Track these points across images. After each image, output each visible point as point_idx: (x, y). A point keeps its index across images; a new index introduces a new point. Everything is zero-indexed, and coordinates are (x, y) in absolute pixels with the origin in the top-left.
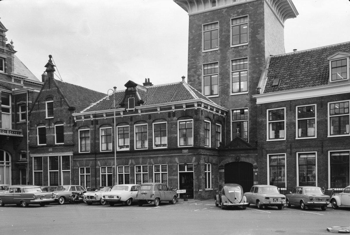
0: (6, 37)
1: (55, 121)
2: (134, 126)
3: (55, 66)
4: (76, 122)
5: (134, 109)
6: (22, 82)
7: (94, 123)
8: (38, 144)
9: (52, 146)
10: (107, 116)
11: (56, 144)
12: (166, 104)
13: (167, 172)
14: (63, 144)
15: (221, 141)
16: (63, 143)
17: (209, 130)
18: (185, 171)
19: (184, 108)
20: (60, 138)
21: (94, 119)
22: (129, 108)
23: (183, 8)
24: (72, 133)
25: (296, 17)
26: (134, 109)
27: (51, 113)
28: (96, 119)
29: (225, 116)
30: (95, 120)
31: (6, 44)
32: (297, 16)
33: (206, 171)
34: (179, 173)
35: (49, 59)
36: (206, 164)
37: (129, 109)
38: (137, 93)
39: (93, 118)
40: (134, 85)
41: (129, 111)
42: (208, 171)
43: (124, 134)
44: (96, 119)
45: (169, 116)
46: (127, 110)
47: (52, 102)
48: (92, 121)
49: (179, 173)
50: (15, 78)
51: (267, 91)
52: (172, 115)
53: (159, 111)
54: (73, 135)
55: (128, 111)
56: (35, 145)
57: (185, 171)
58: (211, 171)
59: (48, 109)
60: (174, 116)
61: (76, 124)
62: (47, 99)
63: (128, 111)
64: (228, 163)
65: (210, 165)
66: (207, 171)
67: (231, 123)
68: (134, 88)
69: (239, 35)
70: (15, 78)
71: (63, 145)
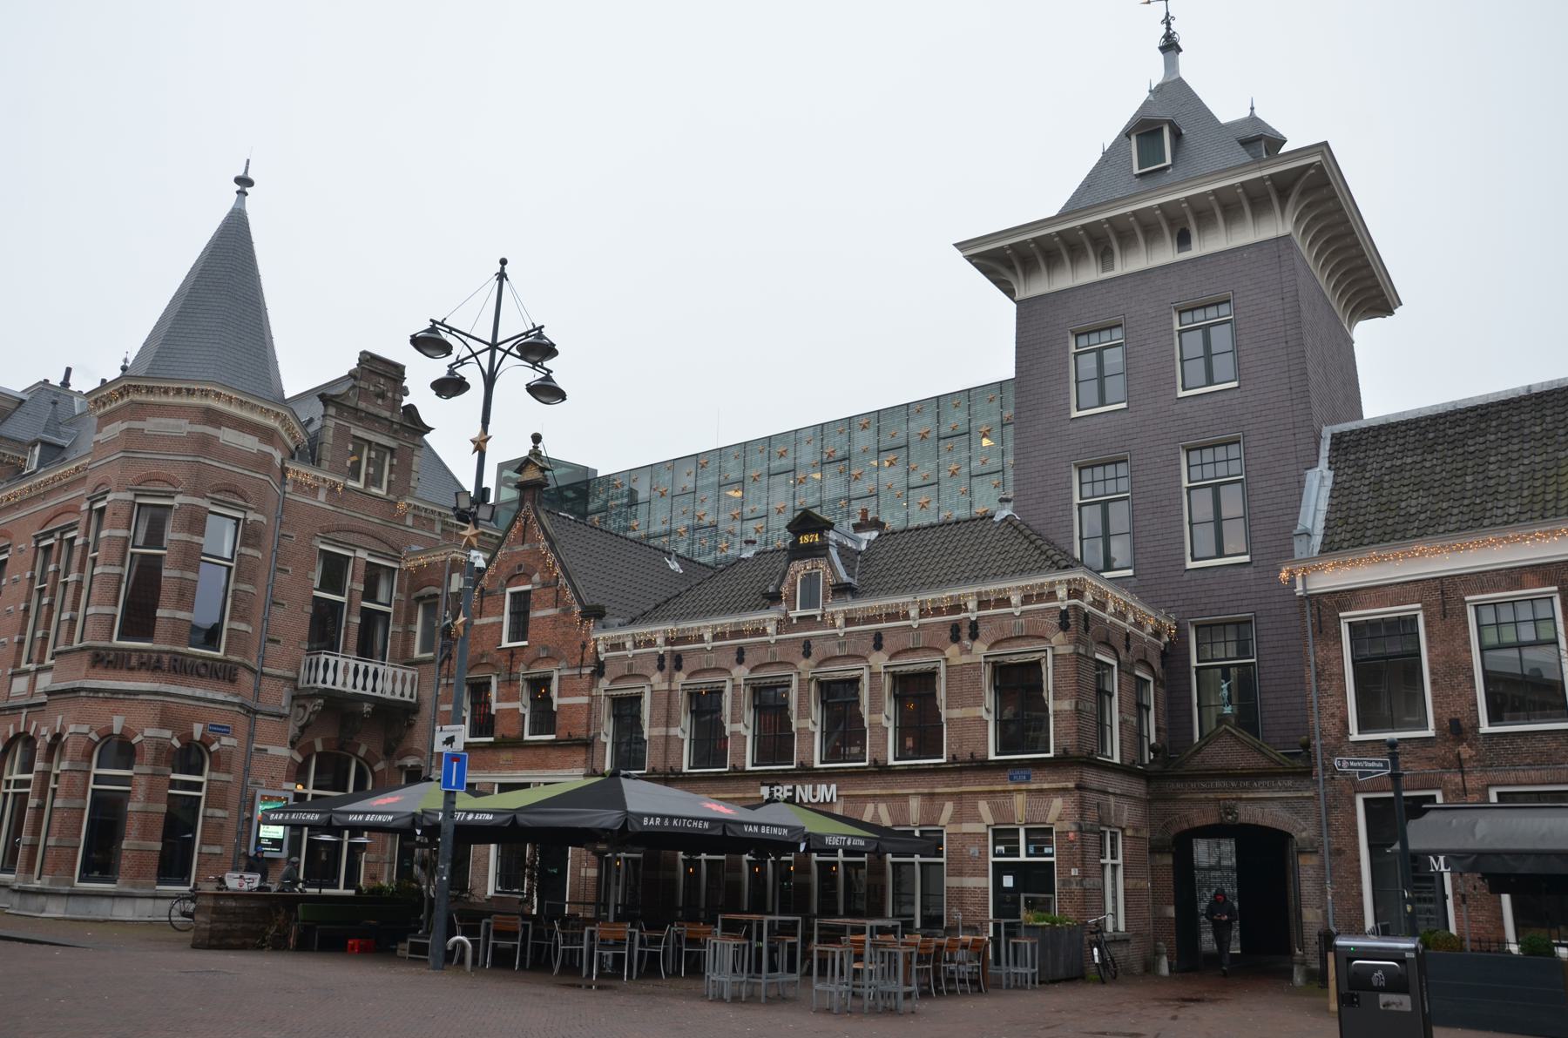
0: (404, 384)
1: (529, 654)
2: (584, 929)
3: (549, 470)
4: (602, 659)
5: (817, 612)
6: (438, 528)
7: (667, 663)
8: (527, 737)
9: (517, 743)
10: (715, 637)
11: (527, 737)
12: (946, 595)
13: (944, 860)
14: (552, 741)
15: (1153, 740)
16: (552, 737)
17: (1111, 695)
18: (1018, 856)
19: (1016, 607)
20: (544, 717)
21: (669, 648)
22: (798, 610)
23: (995, 282)
24: (584, 700)
25: (1391, 313)
26: (817, 612)
27: (520, 628)
28: (676, 648)
29: (1165, 644)
30: (673, 651)
31: (403, 404)
32: (1395, 311)
33: (1104, 858)
34: (993, 863)
35: (531, 445)
36: (1102, 829)
37: (799, 612)
38: (833, 552)
39: (666, 645)
40: (822, 525)
41: (799, 618)
42: (1112, 858)
43: (850, 500)
44: (676, 648)
45: (955, 638)
46: (792, 614)
47: (528, 592)
48: (661, 658)
49: (993, 863)
50: (416, 512)
51: (1329, 547)
52: (965, 631)
53: (915, 620)
54: (589, 705)
55: (795, 621)
56: (130, 736)
57: (1018, 856)
58: (1120, 860)
59: (511, 613)
60: (974, 636)
61: (604, 667)
62: (514, 580)
63: (795, 621)
64: (1186, 826)
65: (1116, 833)
66: (1108, 860)
67: (1194, 671)
68: (821, 536)
69: (1202, 359)
70: (416, 512)
71: (550, 744)
